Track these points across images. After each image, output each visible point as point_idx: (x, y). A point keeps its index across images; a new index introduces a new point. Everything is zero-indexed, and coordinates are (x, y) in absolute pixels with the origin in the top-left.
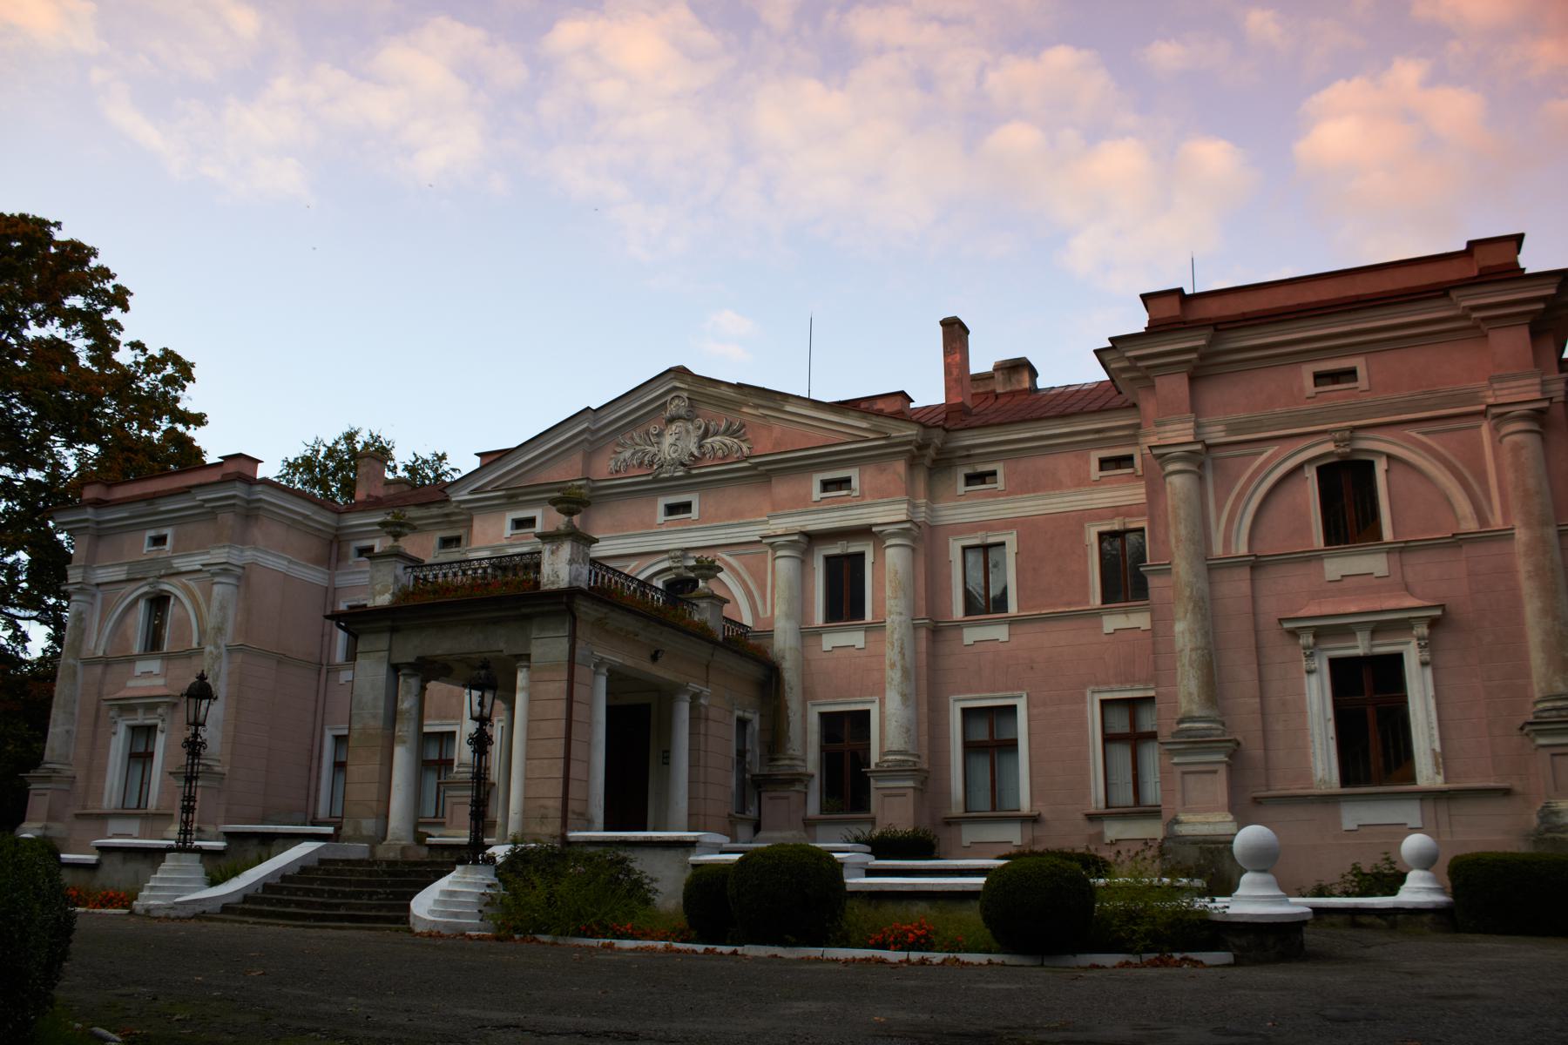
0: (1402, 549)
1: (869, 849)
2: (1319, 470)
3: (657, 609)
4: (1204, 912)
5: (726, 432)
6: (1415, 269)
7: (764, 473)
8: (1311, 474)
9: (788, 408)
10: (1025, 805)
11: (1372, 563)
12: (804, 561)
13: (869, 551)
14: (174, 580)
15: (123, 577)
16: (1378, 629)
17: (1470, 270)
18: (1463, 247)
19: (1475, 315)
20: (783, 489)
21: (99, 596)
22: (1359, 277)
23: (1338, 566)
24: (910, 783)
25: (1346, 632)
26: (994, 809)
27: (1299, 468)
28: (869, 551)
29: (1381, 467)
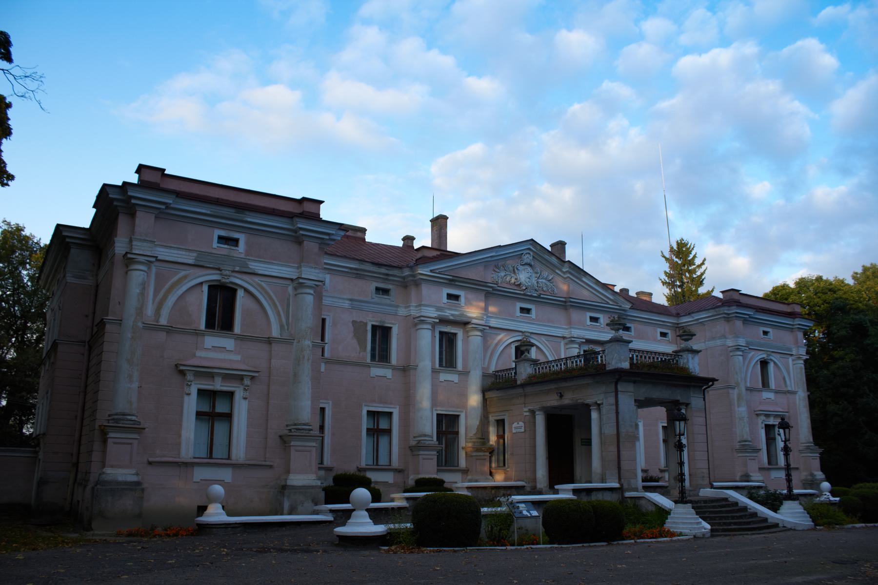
0: (241, 338)
1: (446, 485)
2: (210, 287)
3: (581, 368)
4: (386, 523)
5: (546, 279)
6: (217, 189)
7: (567, 304)
8: (205, 288)
9: (584, 279)
10: (395, 463)
11: (228, 343)
12: (433, 330)
13: (460, 333)
14: (245, 277)
15: (191, 262)
16: (227, 377)
17: (296, 209)
18: (299, 197)
19: (302, 232)
20: (575, 315)
21: (154, 269)
22: (243, 194)
23: (212, 340)
24: (314, 444)
25: (211, 376)
26: (211, 457)
27: (201, 283)
28: (460, 333)
29: (240, 293)
